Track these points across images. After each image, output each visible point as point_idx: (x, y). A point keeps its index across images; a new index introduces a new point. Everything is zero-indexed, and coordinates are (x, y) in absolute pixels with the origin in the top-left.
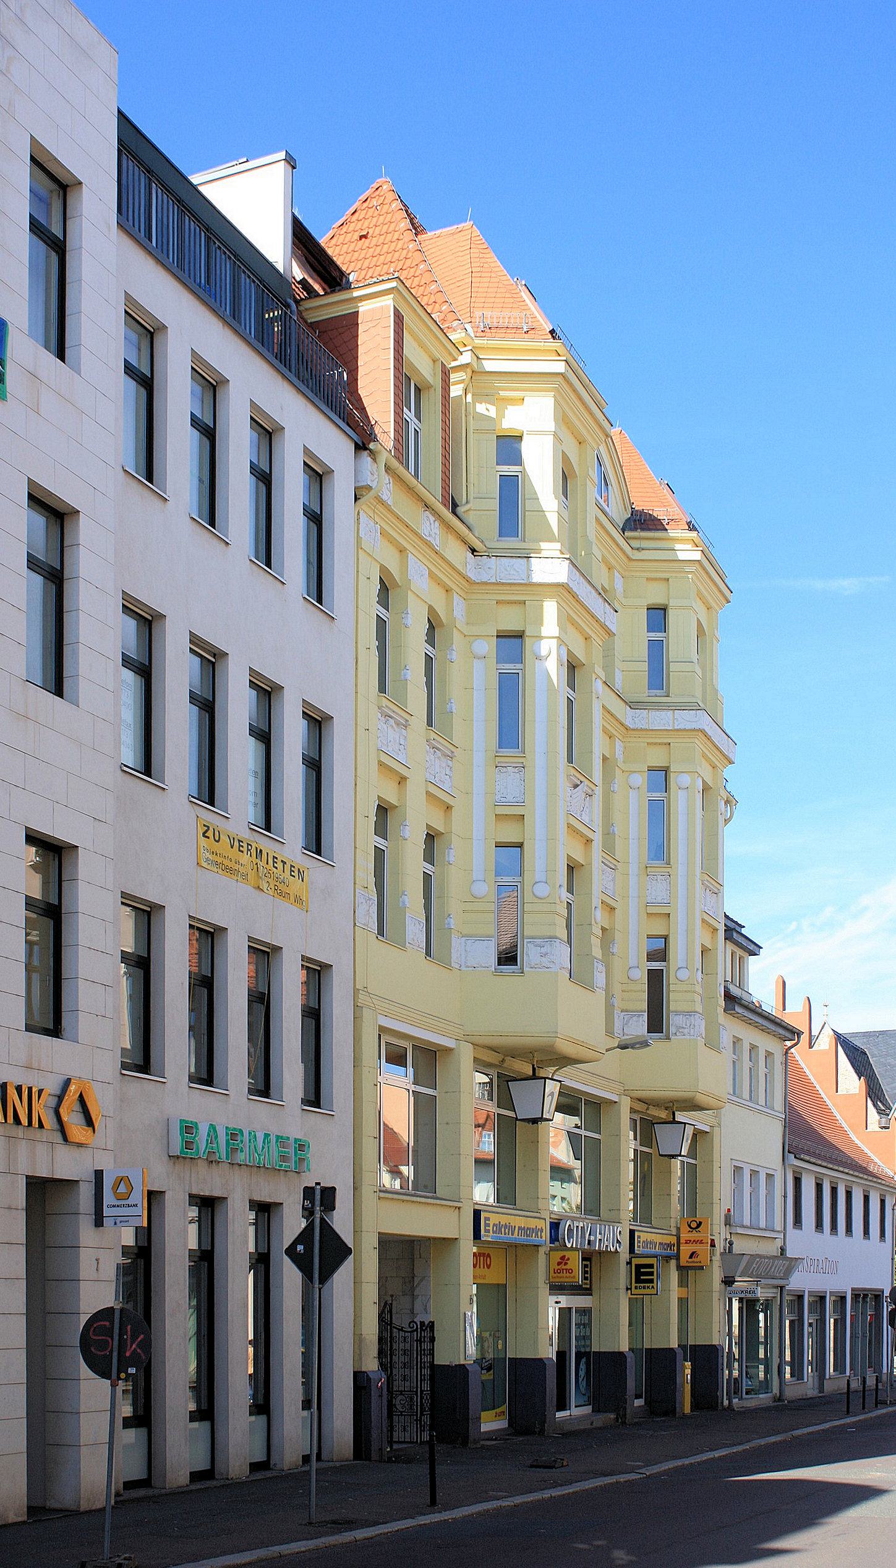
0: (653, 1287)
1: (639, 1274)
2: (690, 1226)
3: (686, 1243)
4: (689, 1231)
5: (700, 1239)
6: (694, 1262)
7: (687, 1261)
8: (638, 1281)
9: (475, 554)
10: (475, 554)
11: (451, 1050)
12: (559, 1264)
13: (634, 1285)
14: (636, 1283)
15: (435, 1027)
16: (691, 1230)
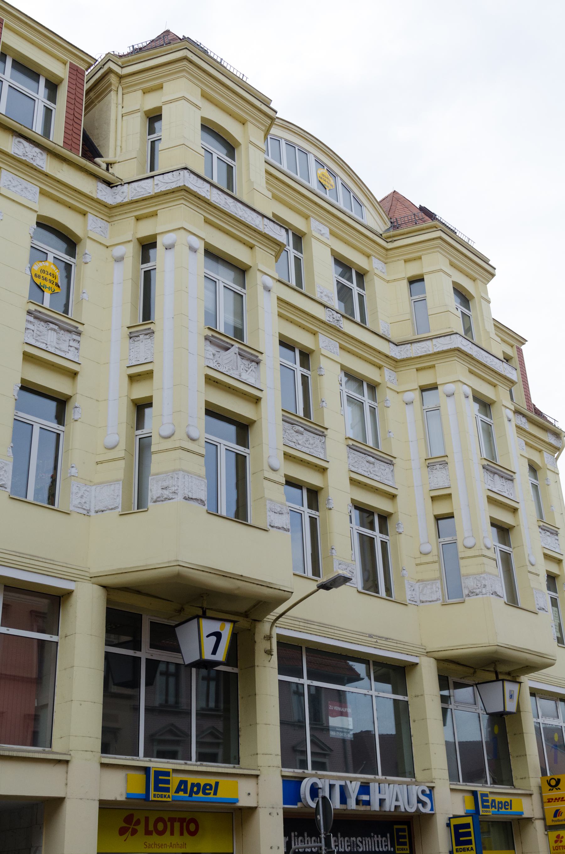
0: (472, 849)
1: (458, 836)
2: (549, 784)
3: (549, 802)
4: (550, 790)
5: (561, 797)
6: (559, 821)
7: (553, 821)
8: (458, 843)
9: (111, 186)
10: (111, 186)
11: (417, 664)
12: (556, 842)
13: (455, 848)
14: (456, 845)
15: (327, 633)
16: (552, 788)
